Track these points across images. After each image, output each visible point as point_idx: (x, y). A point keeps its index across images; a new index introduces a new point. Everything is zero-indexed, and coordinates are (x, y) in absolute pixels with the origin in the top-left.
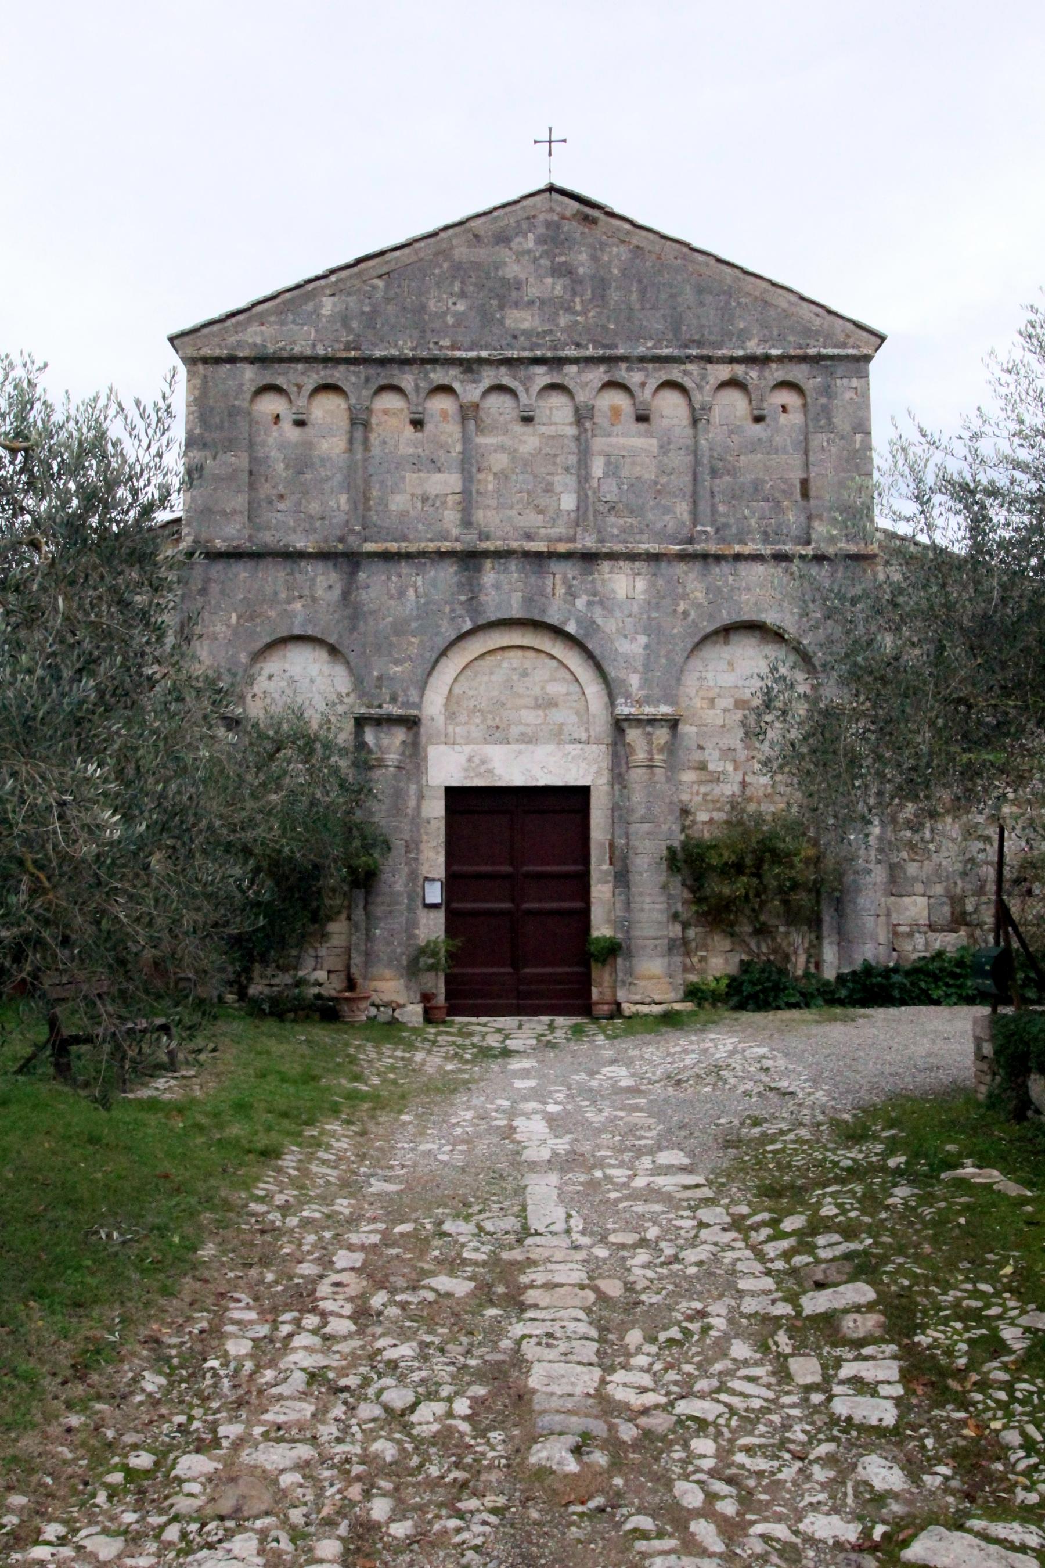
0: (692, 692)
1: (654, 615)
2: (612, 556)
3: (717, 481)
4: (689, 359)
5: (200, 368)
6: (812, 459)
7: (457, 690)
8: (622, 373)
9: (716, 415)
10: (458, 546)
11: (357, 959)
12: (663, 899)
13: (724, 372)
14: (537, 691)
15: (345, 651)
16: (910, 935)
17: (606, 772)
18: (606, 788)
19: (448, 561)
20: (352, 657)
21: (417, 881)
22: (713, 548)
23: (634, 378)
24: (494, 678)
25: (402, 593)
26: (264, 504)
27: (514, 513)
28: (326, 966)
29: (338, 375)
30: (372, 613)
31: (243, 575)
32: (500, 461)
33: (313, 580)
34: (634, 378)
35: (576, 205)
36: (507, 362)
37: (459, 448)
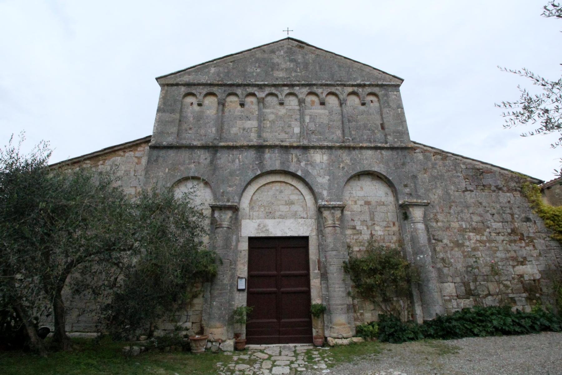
0: (348, 199)
1: (331, 168)
2: (314, 147)
3: (350, 124)
4: (338, 85)
5: (166, 88)
6: (384, 116)
7: (254, 198)
8: (315, 89)
9: (348, 103)
10: (256, 144)
11: (205, 317)
12: (343, 286)
13: (350, 89)
14: (286, 198)
15: (210, 182)
16: (450, 301)
17: (315, 230)
18: (315, 237)
19: (252, 150)
20: (212, 184)
21: (235, 278)
22: (352, 144)
23: (319, 91)
24: (269, 193)
25: (233, 161)
26: (184, 131)
27: (277, 134)
28: (191, 320)
29: (215, 90)
30: (221, 168)
31: (173, 154)
32: (272, 117)
33: (199, 156)
34: (319, 91)
35: (297, 43)
36: (274, 86)
37: (257, 113)
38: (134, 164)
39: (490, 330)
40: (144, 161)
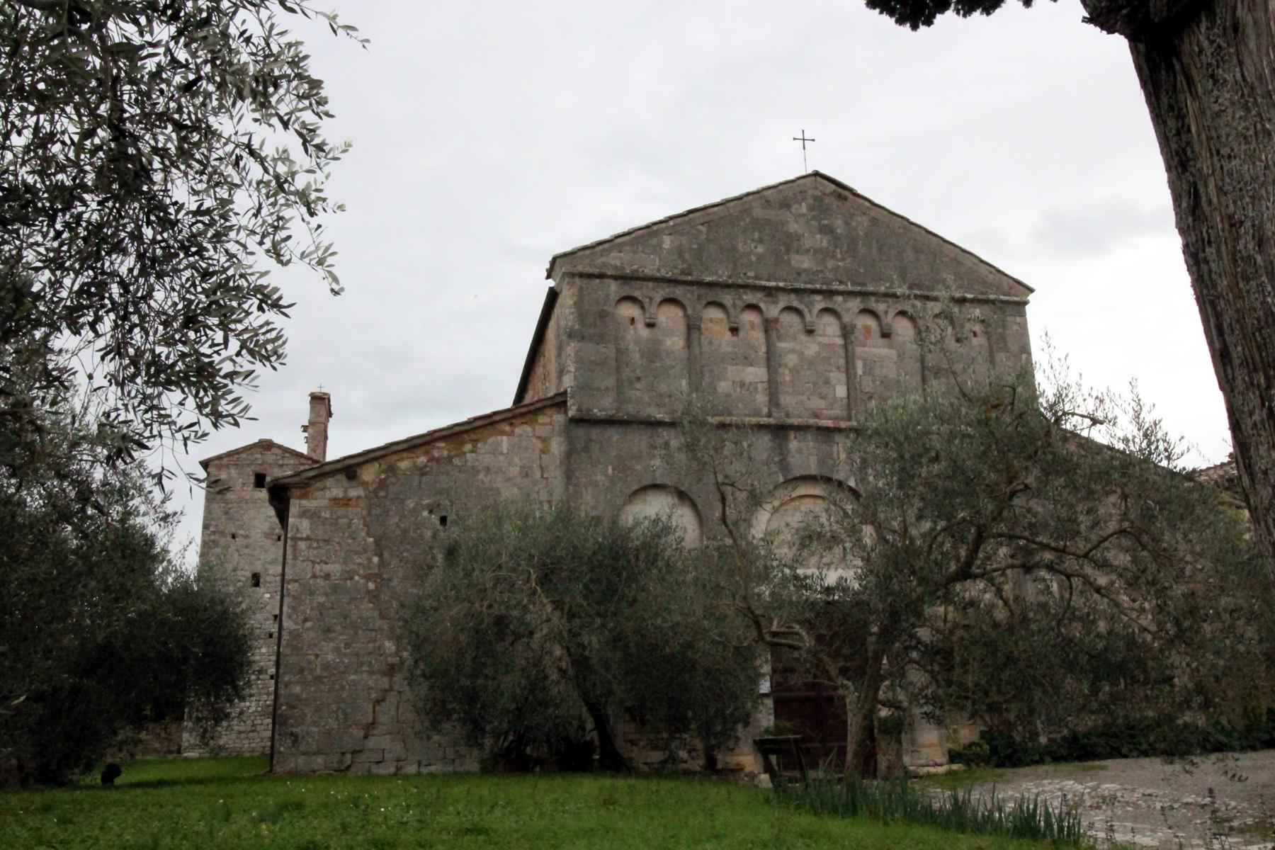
29: (678, 292)
31: (616, 437)
34: (880, 307)
35: (833, 187)
36: (796, 291)
38: (537, 452)
39: (1145, 746)
40: (557, 446)
